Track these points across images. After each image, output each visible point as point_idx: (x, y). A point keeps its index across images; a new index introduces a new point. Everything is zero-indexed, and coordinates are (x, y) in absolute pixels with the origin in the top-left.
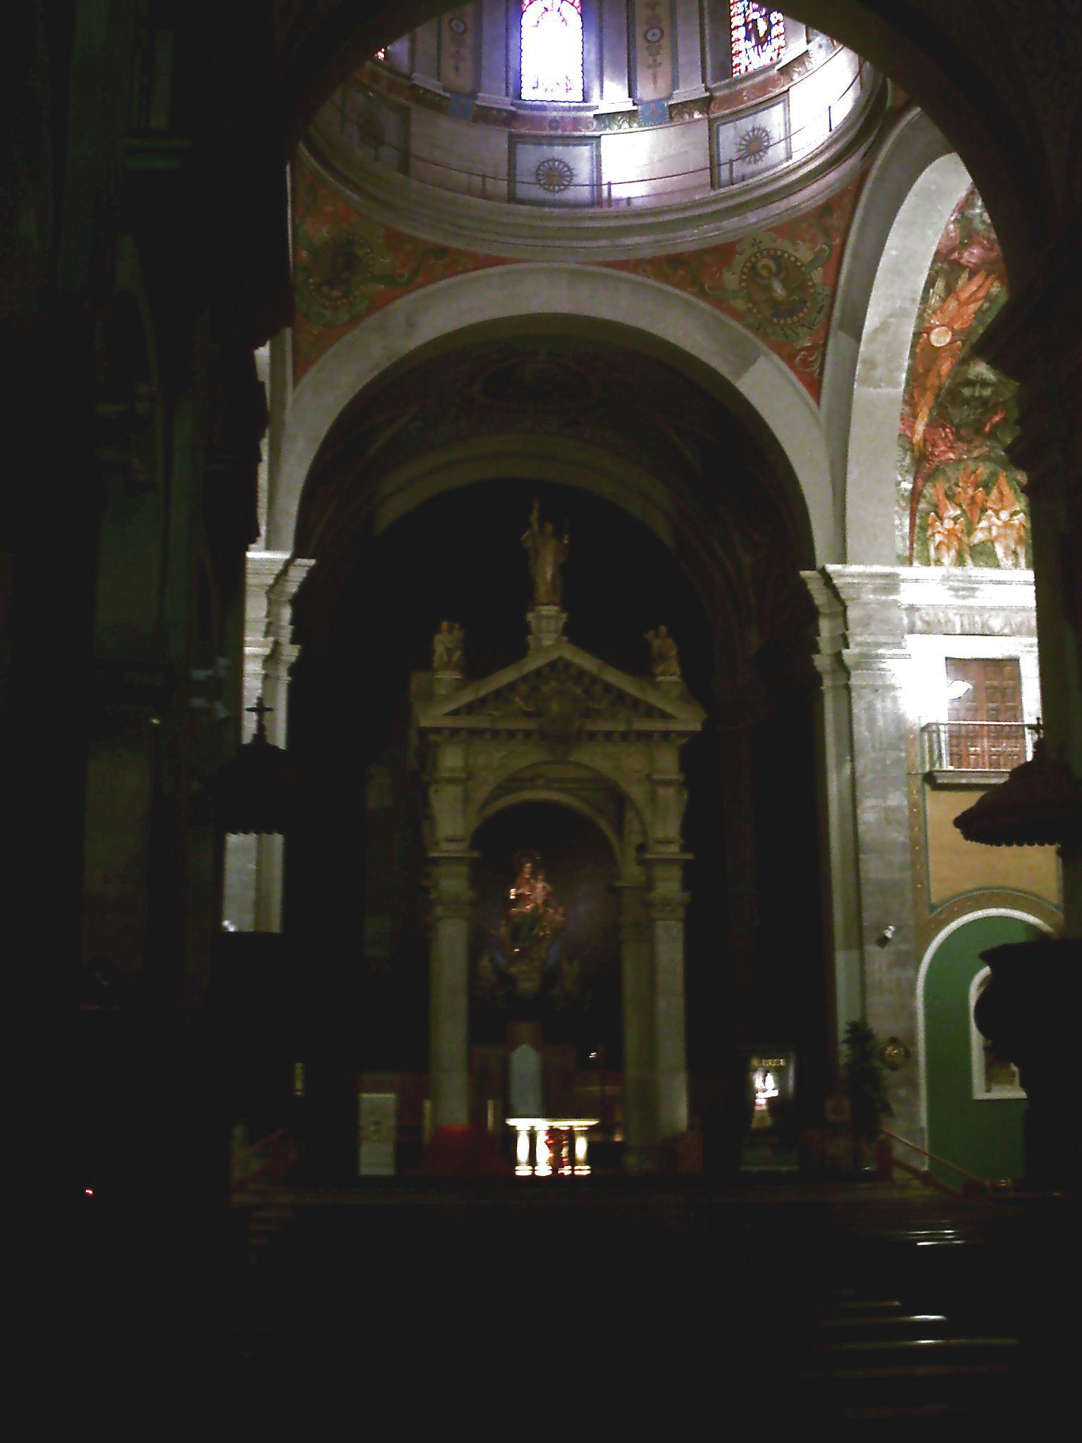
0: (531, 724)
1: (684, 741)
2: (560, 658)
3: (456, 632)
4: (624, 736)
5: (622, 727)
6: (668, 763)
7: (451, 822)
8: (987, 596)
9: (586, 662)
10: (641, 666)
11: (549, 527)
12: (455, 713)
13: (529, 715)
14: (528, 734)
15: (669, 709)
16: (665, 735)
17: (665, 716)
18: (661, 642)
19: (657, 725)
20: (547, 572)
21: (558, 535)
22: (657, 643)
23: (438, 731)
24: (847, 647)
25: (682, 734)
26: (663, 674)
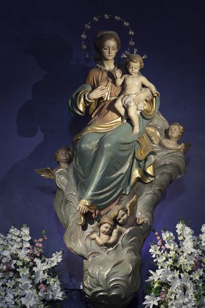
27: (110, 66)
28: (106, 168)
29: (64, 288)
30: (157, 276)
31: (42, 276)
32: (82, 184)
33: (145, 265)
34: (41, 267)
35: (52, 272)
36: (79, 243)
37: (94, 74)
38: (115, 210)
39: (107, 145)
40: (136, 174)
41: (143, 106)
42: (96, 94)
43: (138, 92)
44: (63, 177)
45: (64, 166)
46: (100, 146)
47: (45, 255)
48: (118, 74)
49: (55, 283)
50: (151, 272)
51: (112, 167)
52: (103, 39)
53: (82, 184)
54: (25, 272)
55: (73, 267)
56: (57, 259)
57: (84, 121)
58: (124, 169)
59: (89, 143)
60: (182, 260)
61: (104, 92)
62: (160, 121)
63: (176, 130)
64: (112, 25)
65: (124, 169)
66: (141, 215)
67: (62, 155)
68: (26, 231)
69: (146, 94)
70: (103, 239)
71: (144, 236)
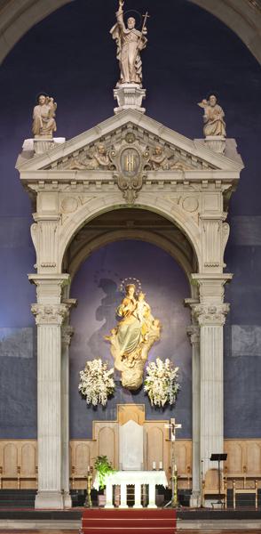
0: (109, 177)
1: (227, 187)
2: (129, 122)
3: (51, 104)
4: (180, 182)
5: (179, 177)
6: (214, 205)
7: (50, 245)
8: (131, 430)
9: (152, 127)
10: (194, 129)
11: (132, 21)
12: (48, 167)
13: (108, 168)
14: (105, 182)
15: (214, 162)
16: (212, 181)
17: (212, 167)
18: (212, 109)
19: (206, 175)
20: (130, 52)
21: (138, 27)
22: (208, 110)
23: (36, 182)
24: (197, 272)
25: (224, 182)
26: (212, 134)
27: (131, 297)
28: (248, 50)
29: (115, 382)
30: (148, 379)
31: (106, 378)
32: (121, 342)
33: (145, 374)
34: (106, 375)
35: (111, 376)
36: (120, 365)
37: (126, 300)
38: (134, 354)
39: (130, 330)
40: (142, 340)
41: (144, 314)
42: (126, 309)
43: (142, 307)
44: (114, 340)
45: (114, 336)
46: (128, 329)
47: (108, 369)
48: (134, 301)
49: (111, 381)
50: (229, 276)
51: (132, 339)
52: (128, 287)
53: (121, 342)
54: (100, 377)
55: (118, 373)
56: (112, 371)
57: (120, 319)
58: (137, 339)
59: (124, 326)
60: (158, 373)
61: (130, 307)
62: (151, 318)
63: (157, 322)
64: (135, 282)
65: (137, 339)
66: (144, 356)
67: (114, 332)
68: (100, 361)
69: (145, 309)
70: (129, 365)
71: (145, 363)
